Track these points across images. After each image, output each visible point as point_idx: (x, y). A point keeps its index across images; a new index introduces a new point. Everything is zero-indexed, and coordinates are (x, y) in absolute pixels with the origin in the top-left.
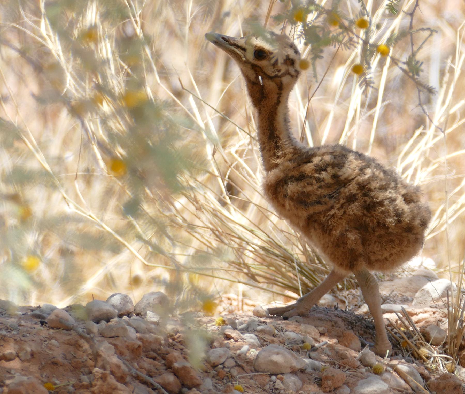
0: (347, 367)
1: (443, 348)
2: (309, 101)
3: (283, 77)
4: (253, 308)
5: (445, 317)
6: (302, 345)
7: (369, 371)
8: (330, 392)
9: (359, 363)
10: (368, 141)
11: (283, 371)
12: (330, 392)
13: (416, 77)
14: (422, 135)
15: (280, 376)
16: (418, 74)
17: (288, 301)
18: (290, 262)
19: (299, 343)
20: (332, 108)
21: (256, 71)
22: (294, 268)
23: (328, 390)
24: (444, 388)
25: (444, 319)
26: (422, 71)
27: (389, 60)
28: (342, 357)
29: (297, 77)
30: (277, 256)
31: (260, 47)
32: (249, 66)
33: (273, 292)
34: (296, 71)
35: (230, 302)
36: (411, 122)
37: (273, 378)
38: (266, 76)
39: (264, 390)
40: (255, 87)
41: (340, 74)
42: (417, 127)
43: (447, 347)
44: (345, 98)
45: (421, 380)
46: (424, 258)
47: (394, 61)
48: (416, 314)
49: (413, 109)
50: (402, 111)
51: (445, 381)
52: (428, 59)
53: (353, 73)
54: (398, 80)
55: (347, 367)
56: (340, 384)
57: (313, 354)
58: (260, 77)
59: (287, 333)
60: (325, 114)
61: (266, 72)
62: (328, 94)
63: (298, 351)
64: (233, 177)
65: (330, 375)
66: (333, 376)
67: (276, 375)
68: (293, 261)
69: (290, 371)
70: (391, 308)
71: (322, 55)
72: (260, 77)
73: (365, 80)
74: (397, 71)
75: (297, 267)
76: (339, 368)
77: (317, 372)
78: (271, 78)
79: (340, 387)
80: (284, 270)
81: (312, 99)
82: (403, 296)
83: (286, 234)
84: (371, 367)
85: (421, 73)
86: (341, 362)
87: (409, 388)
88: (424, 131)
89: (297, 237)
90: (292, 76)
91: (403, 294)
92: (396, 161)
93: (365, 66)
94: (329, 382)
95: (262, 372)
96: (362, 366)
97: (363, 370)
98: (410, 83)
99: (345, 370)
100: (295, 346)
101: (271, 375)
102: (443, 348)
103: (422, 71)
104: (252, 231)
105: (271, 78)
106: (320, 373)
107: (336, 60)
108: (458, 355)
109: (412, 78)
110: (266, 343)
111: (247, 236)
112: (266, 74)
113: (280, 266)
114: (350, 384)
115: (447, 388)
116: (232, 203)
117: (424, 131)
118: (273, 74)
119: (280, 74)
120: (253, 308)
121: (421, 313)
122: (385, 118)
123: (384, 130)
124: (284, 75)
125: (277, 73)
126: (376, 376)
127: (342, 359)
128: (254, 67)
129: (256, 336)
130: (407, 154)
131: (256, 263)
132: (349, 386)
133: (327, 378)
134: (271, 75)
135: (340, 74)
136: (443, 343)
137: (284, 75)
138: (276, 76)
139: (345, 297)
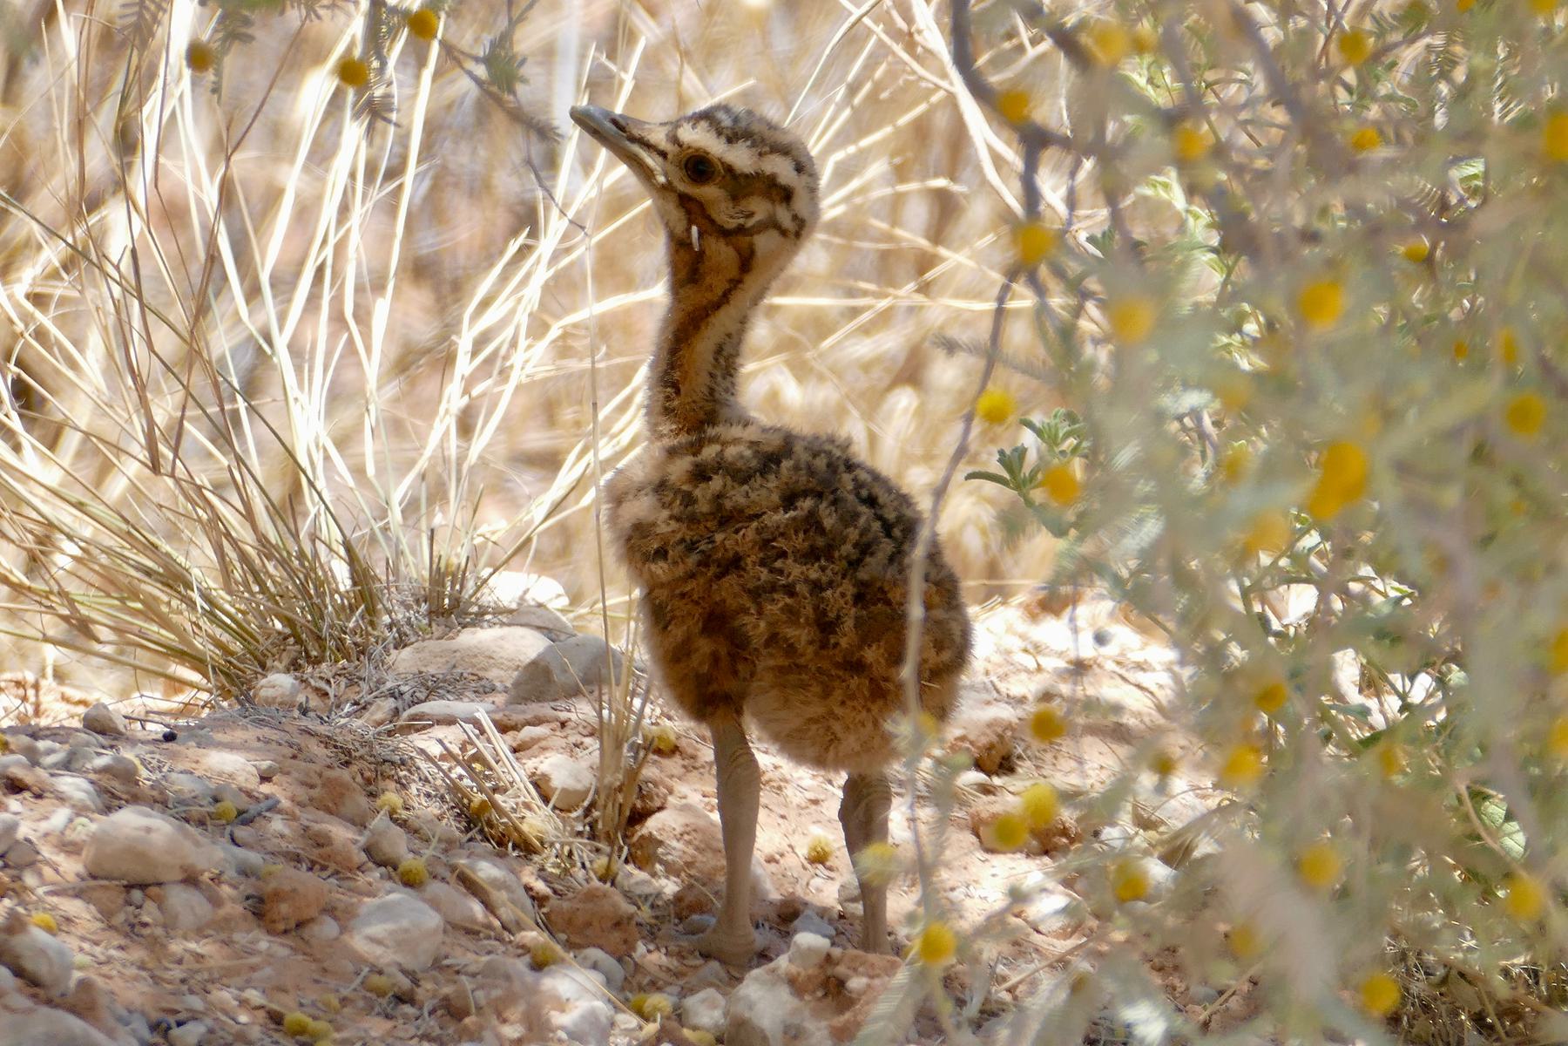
0: (332, 867)
1: (586, 816)
2: (228, 159)
3: (759, 232)
4: (81, 710)
5: (591, 735)
6: (212, 809)
7: (390, 878)
8: (286, 932)
9: (364, 857)
10: (387, 267)
11: (162, 879)
12: (286, 932)
13: (508, 97)
14: (525, 251)
15: (154, 890)
16: (512, 91)
17: (177, 691)
18: (182, 589)
19: (204, 802)
20: (292, 179)
21: (688, 212)
22: (192, 604)
23: (281, 927)
24: (589, 924)
25: (588, 741)
26: (524, 81)
27: (435, 49)
28: (321, 841)
29: (798, 235)
30: (148, 573)
31: (697, 150)
32: (673, 198)
33: (135, 668)
34: (795, 217)
35: (21, 692)
36: (502, 219)
37: (137, 895)
38: (712, 228)
39: (111, 927)
40: (682, 252)
41: (318, 86)
42: (515, 233)
43: (596, 814)
44: (322, 153)
45: (528, 902)
46: (534, 577)
47: (450, 52)
48: (99, 642)
49: (508, 183)
50: (480, 189)
51: (590, 906)
52: (548, 53)
53: (344, 85)
54: (469, 102)
55: (332, 867)
56: (313, 912)
57: (242, 833)
58: (694, 229)
59: (174, 776)
60: (273, 196)
61: (714, 216)
62: (279, 139)
63: (201, 823)
64: (29, 358)
65: (287, 888)
66: (294, 890)
67: (143, 886)
68: (189, 586)
69: (180, 877)
70: (448, 711)
71: (250, 31)
72: (694, 229)
73: (370, 102)
74: (463, 86)
75: (199, 601)
76: (310, 869)
77: (253, 879)
78: (725, 234)
79: (312, 920)
80: (165, 609)
81: (233, 159)
82: (480, 679)
83: (170, 515)
84: (395, 869)
85: (520, 88)
86: (315, 853)
87: (497, 923)
88: (530, 242)
89: (200, 520)
90: (784, 233)
91: (481, 674)
92: (459, 322)
93: (376, 64)
94: (284, 908)
95: (106, 878)
96: (370, 864)
97: (376, 874)
98: (499, 119)
99: (325, 874)
100: (195, 810)
101: (129, 887)
102: (586, 816)
103: (524, 81)
104: (79, 506)
105: (725, 234)
106: (261, 883)
107: (300, 53)
108: (625, 837)
109: (499, 101)
110: (117, 802)
111: (65, 515)
112: (712, 221)
113: (156, 599)
114: (338, 913)
115: (596, 923)
116: (28, 431)
117: (530, 242)
118: (731, 224)
119: (750, 223)
120: (81, 710)
121: (529, 724)
122: (432, 209)
123: (428, 242)
124: (763, 227)
125: (741, 221)
126: (408, 890)
127: (319, 845)
128: (684, 201)
129: (92, 782)
130: (485, 304)
131: (93, 592)
132: (336, 918)
133: (277, 896)
134: (728, 226)
135: (318, 86)
136: (586, 803)
137: (763, 227)
138: (741, 230)
139: (328, 682)
